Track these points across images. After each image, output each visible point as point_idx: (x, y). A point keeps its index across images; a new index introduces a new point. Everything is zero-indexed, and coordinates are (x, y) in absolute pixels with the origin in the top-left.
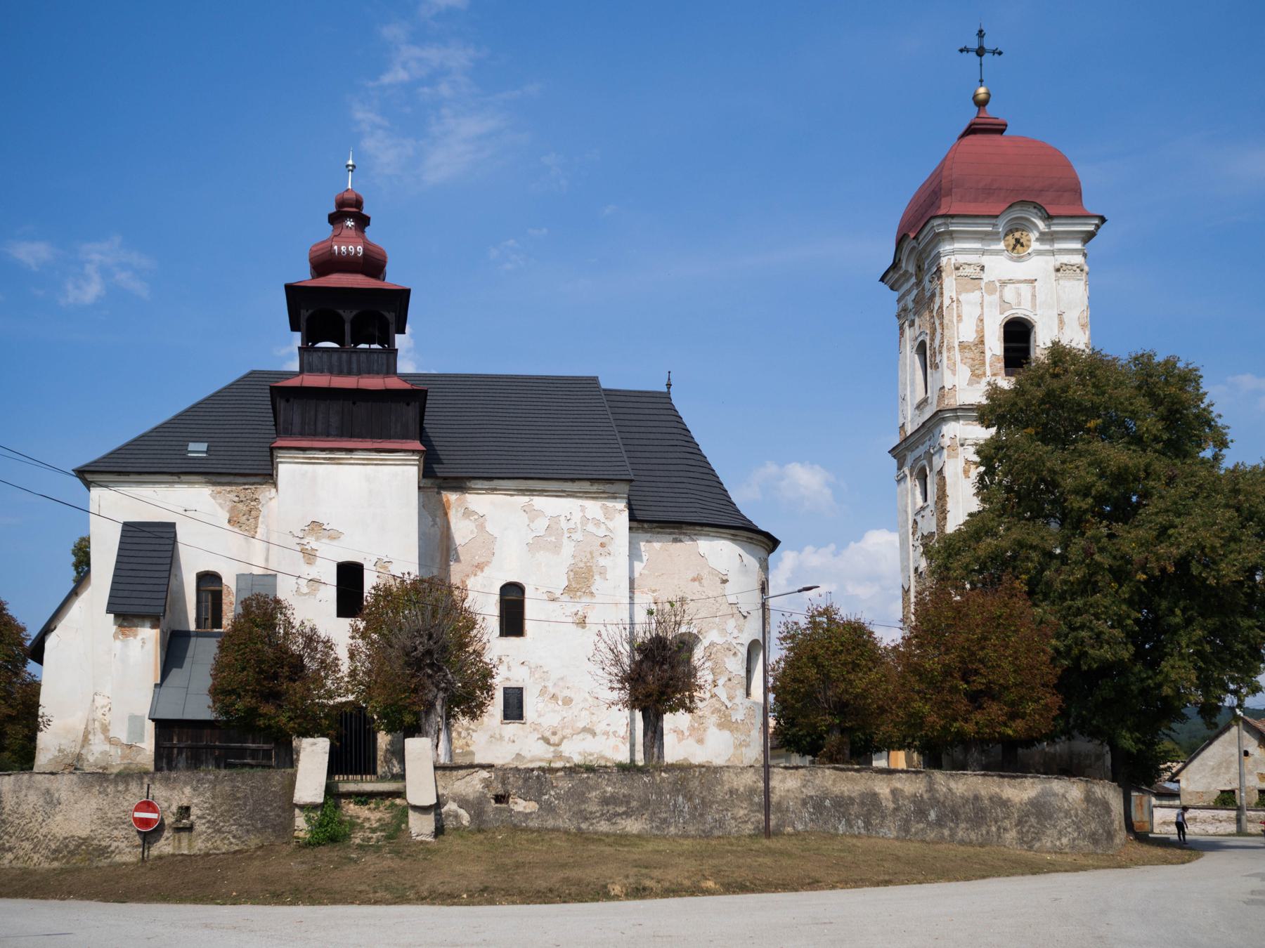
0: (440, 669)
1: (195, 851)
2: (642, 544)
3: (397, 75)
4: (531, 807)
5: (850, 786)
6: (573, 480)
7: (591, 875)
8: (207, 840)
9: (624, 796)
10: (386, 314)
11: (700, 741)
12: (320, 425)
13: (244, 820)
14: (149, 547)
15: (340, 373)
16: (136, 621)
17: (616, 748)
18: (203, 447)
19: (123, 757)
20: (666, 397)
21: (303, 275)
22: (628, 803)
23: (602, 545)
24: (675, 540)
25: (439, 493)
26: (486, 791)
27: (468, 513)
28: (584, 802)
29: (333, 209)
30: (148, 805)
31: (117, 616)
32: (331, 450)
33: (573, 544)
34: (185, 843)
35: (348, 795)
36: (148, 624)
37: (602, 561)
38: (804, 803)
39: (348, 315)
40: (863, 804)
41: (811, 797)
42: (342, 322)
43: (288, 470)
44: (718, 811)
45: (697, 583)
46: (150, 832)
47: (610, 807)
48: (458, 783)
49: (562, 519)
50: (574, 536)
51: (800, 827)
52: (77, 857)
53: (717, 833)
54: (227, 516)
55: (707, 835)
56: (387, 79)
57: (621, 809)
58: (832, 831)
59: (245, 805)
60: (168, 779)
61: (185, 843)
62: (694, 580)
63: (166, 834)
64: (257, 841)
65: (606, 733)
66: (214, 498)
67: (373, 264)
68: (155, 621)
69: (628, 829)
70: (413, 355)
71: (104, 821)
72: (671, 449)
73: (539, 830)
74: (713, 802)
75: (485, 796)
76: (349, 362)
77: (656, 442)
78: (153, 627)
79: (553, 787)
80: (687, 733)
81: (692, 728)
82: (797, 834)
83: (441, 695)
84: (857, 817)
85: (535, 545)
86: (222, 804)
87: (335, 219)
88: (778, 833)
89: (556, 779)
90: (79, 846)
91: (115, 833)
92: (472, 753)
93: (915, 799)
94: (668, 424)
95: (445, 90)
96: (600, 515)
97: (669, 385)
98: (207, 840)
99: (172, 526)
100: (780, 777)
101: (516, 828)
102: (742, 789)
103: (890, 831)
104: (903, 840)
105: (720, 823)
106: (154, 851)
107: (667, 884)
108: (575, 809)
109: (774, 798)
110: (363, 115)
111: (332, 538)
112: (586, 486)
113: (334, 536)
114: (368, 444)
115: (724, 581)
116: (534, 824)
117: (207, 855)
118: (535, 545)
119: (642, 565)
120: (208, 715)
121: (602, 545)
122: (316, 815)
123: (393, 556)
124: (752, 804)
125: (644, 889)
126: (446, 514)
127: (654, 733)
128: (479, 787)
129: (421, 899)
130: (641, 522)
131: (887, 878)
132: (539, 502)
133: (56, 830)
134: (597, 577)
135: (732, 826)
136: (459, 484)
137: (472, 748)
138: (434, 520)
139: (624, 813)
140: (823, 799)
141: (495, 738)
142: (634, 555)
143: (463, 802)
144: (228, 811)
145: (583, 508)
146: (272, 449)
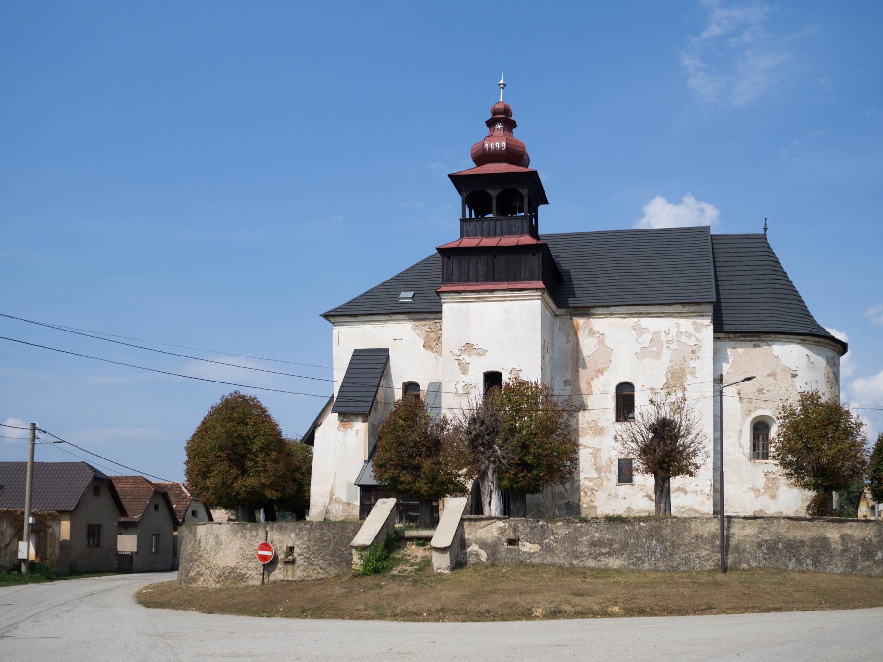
0: (491, 447)
1: (296, 578)
2: (729, 350)
3: (715, 30)
4: (535, 548)
5: (802, 533)
6: (669, 304)
7: (522, 601)
8: (304, 570)
9: (608, 540)
10: (521, 190)
11: (773, 497)
12: (471, 274)
13: (327, 557)
14: (371, 365)
15: (489, 235)
16: (352, 417)
17: (702, 503)
18: (410, 294)
19: (344, 511)
20: (764, 237)
21: (466, 166)
22: (611, 545)
23: (693, 352)
24: (755, 346)
25: (571, 319)
26: (501, 536)
27: (592, 333)
28: (576, 545)
29: (490, 116)
30: (265, 546)
31: (340, 414)
32: (479, 291)
33: (670, 352)
34: (290, 572)
35: (412, 539)
36: (360, 419)
37: (692, 364)
38: (760, 545)
39: (494, 193)
40: (813, 546)
41: (766, 541)
42: (490, 198)
43: (450, 308)
44: (685, 552)
45: (772, 378)
46: (270, 564)
47: (597, 548)
48: (481, 530)
49: (662, 334)
50: (672, 346)
51: (754, 564)
52: (229, 581)
53: (682, 568)
54: (423, 342)
55: (675, 570)
56: (706, 35)
57: (605, 550)
58: (783, 567)
59: (329, 546)
60: (281, 528)
61: (290, 572)
62: (769, 375)
63: (279, 566)
64: (336, 571)
65: (695, 492)
66: (414, 330)
67: (515, 155)
68: (365, 417)
69: (610, 565)
70: (551, 221)
71: (245, 557)
72: (761, 277)
73: (538, 566)
74: (681, 545)
75: (500, 539)
76: (495, 227)
77: (750, 273)
78: (363, 421)
79: (553, 533)
80: (762, 491)
81: (767, 488)
82: (751, 569)
83: (492, 466)
84: (807, 557)
85: (641, 355)
86: (314, 546)
87: (491, 123)
88: (735, 568)
89: (556, 527)
90: (230, 573)
91: (250, 564)
92: (595, 507)
93: (863, 542)
94: (761, 258)
95: (747, 37)
96: (691, 330)
97: (766, 229)
98: (304, 570)
99: (387, 350)
100: (740, 525)
101: (521, 563)
102: (706, 535)
103: (837, 567)
104: (850, 574)
105: (686, 561)
106: (272, 578)
107: (579, 608)
108: (569, 550)
109: (733, 542)
110: (689, 62)
111: (479, 355)
112: (680, 308)
113: (481, 353)
114: (505, 286)
115: (794, 376)
116: (536, 561)
117: (303, 580)
118: (641, 355)
119: (729, 366)
120: (375, 483)
121: (693, 352)
122: (367, 553)
123: (524, 363)
124: (713, 547)
125: (560, 612)
126: (576, 334)
127: (662, 492)
128: (496, 533)
129: (395, 617)
130: (722, 330)
131: (778, 605)
132: (645, 322)
133: (219, 562)
134: (688, 376)
135: (696, 563)
136: (585, 311)
137: (595, 504)
138: (567, 339)
139: (607, 553)
140: (776, 543)
141: (612, 496)
142: (718, 357)
143: (483, 545)
144: (318, 550)
145: (678, 325)
146: (438, 293)
